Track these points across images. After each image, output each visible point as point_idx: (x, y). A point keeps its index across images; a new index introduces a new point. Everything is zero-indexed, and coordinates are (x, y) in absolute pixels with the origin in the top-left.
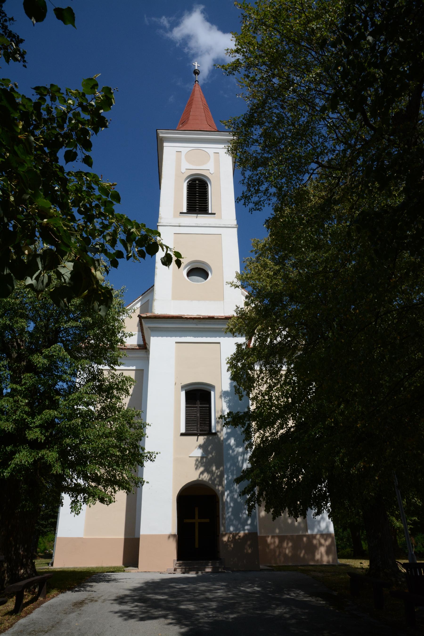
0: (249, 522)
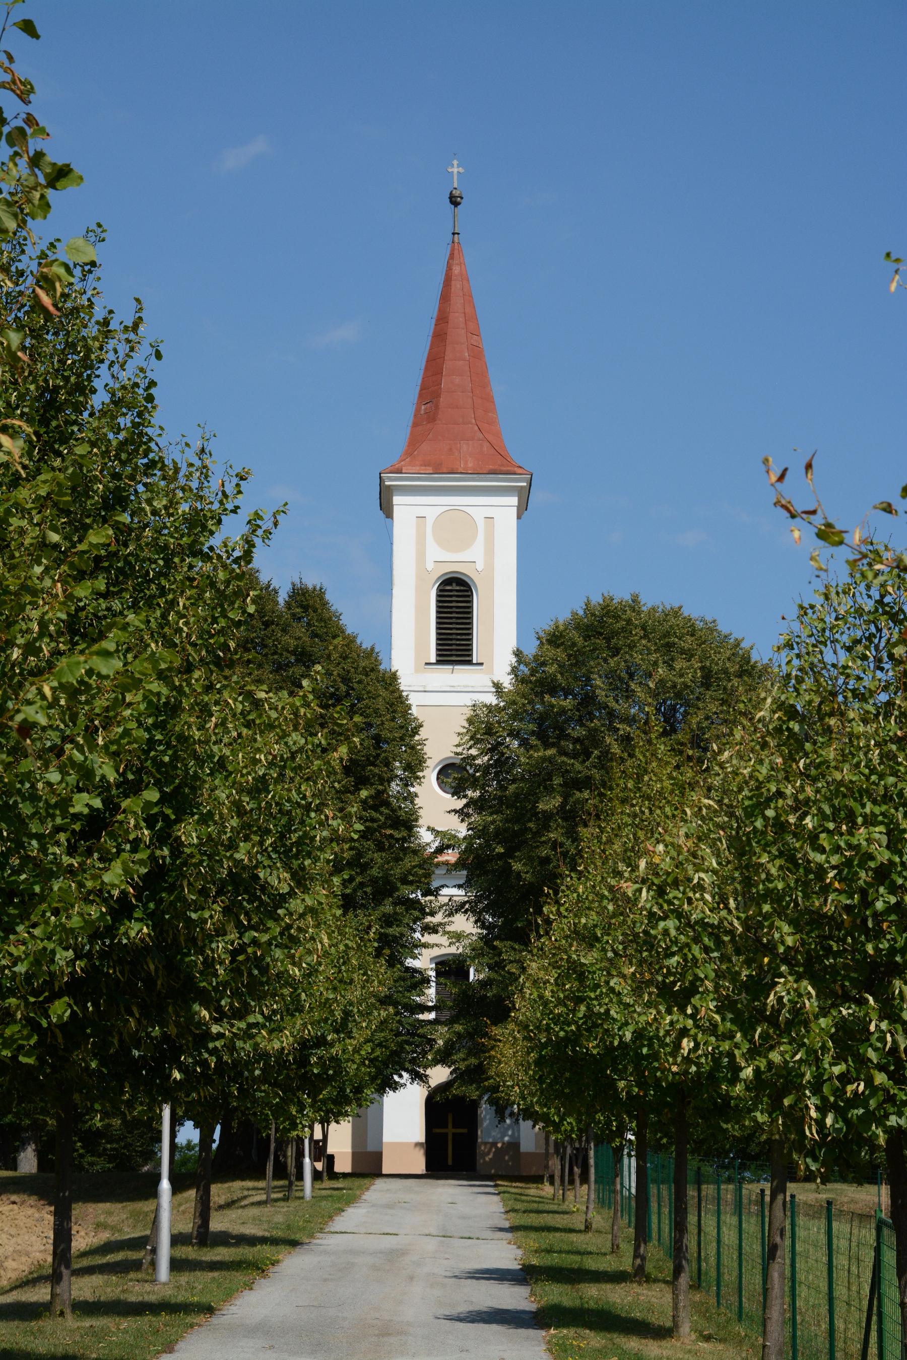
0: (510, 1133)
